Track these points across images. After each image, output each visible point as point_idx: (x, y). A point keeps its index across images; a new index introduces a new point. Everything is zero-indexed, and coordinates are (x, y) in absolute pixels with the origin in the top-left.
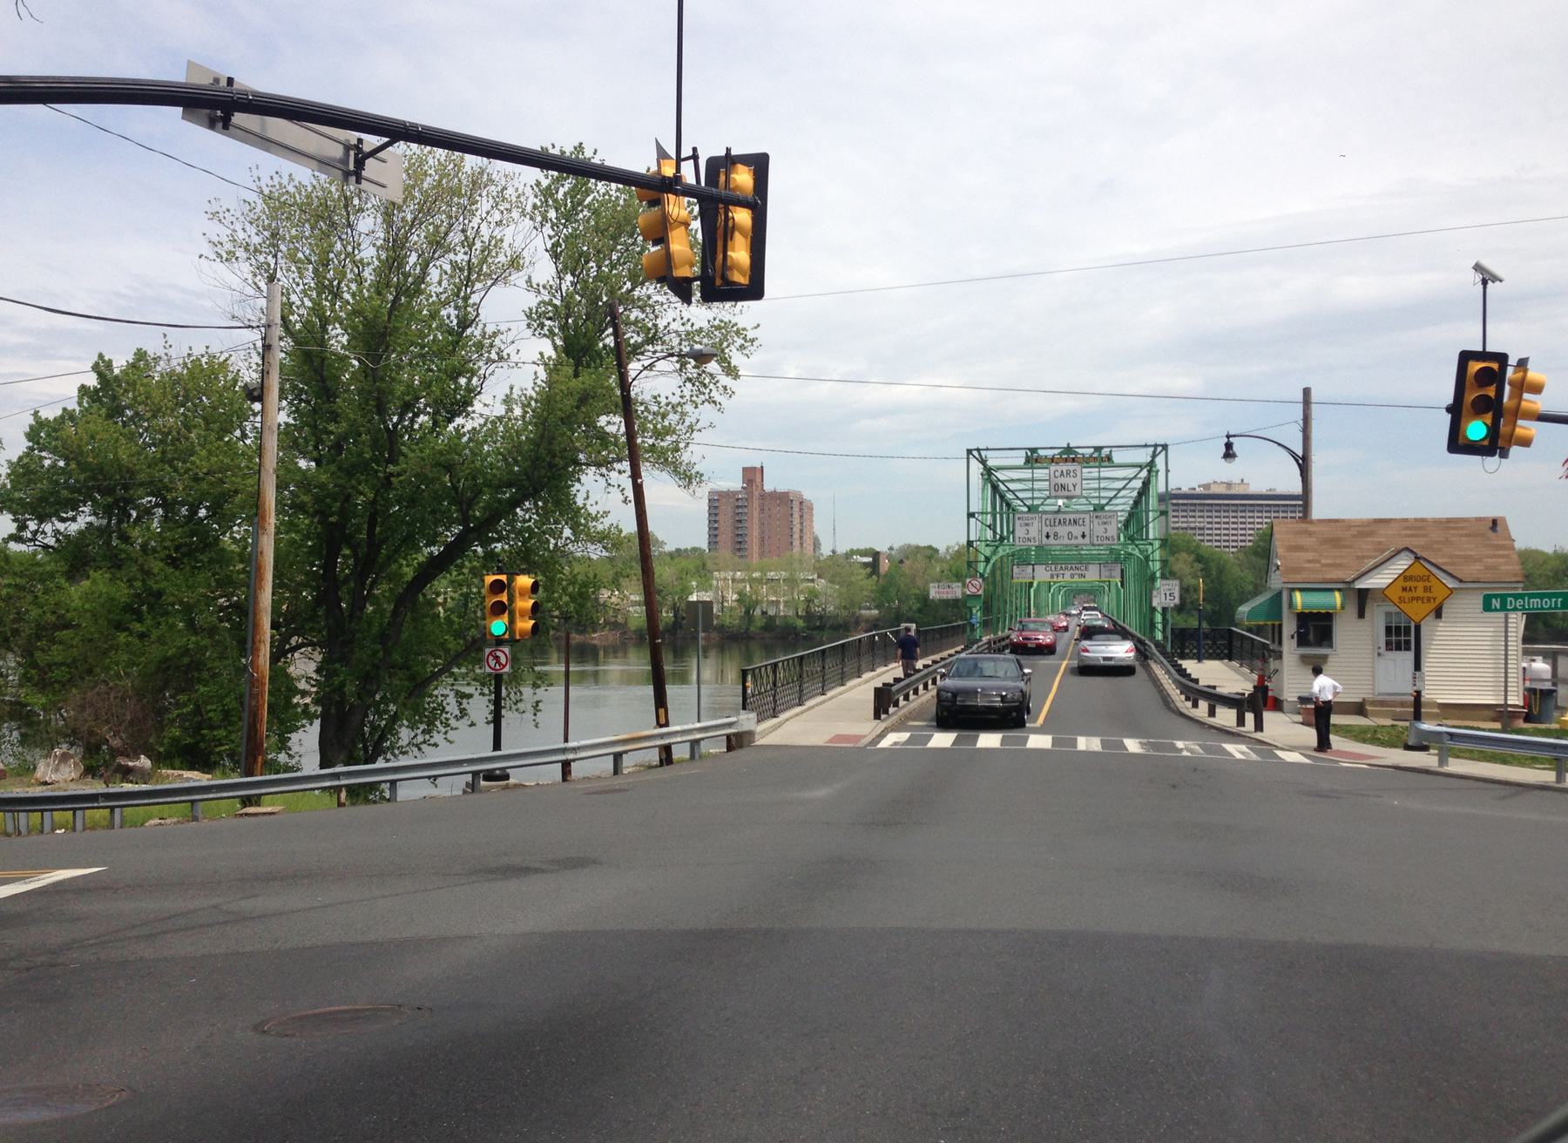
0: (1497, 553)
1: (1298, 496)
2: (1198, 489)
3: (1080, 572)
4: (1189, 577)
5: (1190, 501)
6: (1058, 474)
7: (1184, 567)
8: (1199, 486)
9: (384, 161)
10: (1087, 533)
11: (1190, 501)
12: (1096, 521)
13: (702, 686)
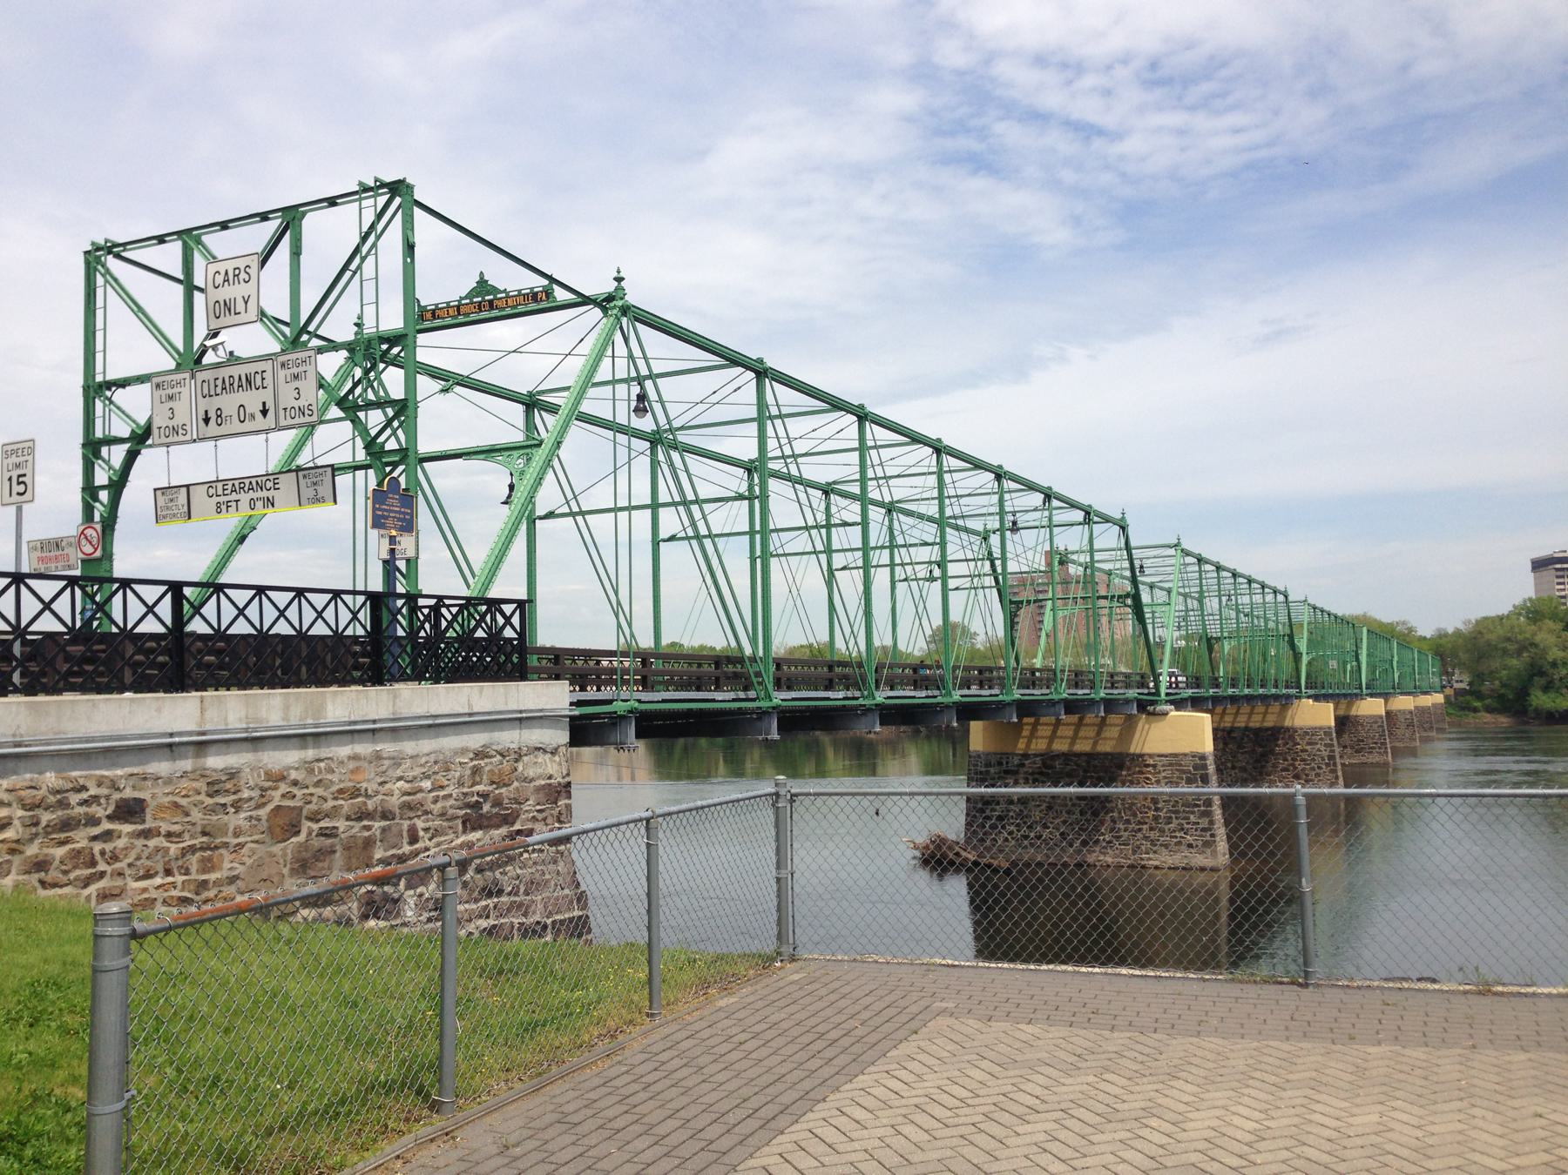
3: (265, 494)
6: (219, 279)
10: (269, 405)
12: (282, 373)
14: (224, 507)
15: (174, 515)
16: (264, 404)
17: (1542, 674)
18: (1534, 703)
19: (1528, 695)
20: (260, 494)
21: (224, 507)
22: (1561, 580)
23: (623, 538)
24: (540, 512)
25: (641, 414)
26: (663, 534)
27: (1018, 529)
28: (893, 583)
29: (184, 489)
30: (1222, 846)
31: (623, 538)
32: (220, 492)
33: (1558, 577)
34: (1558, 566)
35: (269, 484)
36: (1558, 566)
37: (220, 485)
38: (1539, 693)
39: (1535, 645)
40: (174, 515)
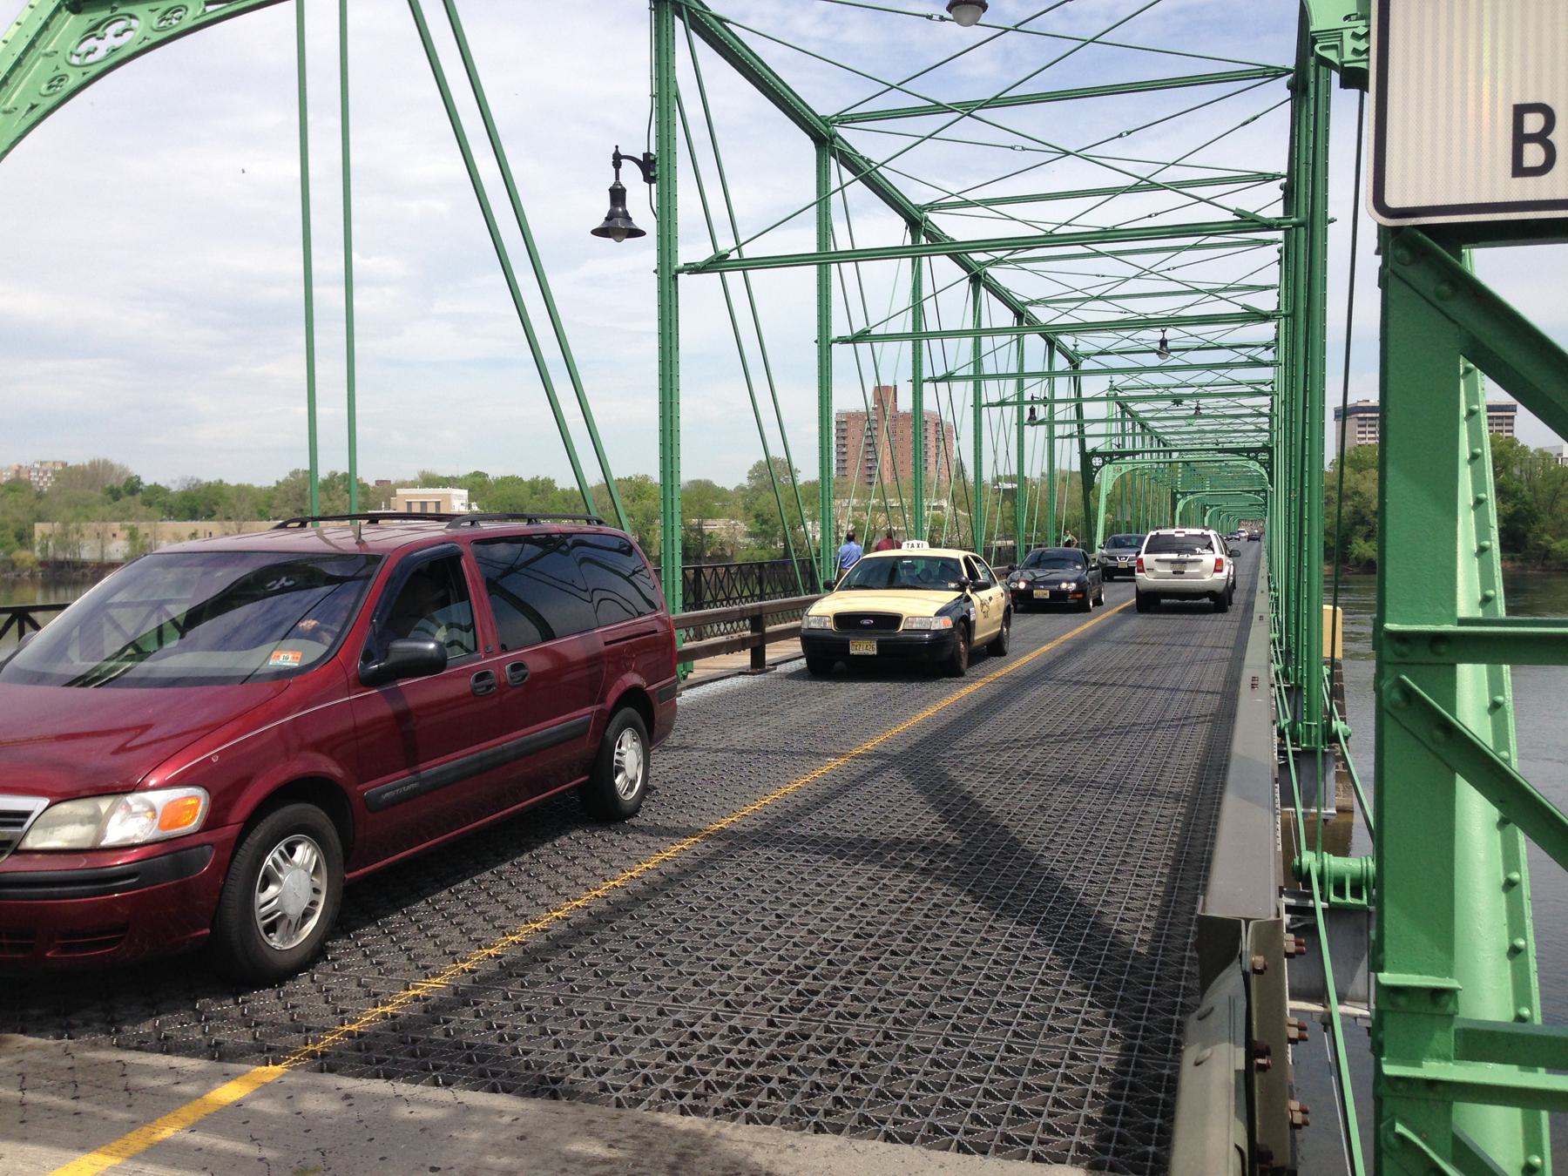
13: (1104, 403)
16: (617, 147)
17: (1363, 521)
18: (1356, 552)
19: (1350, 543)
22: (1363, 429)
23: (329, 297)
24: (680, 264)
26: (839, 328)
28: (978, 407)
30: (1365, 897)
31: (329, 297)
33: (1359, 426)
34: (1361, 415)
36: (1361, 415)
38: (1361, 542)
39: (1356, 493)
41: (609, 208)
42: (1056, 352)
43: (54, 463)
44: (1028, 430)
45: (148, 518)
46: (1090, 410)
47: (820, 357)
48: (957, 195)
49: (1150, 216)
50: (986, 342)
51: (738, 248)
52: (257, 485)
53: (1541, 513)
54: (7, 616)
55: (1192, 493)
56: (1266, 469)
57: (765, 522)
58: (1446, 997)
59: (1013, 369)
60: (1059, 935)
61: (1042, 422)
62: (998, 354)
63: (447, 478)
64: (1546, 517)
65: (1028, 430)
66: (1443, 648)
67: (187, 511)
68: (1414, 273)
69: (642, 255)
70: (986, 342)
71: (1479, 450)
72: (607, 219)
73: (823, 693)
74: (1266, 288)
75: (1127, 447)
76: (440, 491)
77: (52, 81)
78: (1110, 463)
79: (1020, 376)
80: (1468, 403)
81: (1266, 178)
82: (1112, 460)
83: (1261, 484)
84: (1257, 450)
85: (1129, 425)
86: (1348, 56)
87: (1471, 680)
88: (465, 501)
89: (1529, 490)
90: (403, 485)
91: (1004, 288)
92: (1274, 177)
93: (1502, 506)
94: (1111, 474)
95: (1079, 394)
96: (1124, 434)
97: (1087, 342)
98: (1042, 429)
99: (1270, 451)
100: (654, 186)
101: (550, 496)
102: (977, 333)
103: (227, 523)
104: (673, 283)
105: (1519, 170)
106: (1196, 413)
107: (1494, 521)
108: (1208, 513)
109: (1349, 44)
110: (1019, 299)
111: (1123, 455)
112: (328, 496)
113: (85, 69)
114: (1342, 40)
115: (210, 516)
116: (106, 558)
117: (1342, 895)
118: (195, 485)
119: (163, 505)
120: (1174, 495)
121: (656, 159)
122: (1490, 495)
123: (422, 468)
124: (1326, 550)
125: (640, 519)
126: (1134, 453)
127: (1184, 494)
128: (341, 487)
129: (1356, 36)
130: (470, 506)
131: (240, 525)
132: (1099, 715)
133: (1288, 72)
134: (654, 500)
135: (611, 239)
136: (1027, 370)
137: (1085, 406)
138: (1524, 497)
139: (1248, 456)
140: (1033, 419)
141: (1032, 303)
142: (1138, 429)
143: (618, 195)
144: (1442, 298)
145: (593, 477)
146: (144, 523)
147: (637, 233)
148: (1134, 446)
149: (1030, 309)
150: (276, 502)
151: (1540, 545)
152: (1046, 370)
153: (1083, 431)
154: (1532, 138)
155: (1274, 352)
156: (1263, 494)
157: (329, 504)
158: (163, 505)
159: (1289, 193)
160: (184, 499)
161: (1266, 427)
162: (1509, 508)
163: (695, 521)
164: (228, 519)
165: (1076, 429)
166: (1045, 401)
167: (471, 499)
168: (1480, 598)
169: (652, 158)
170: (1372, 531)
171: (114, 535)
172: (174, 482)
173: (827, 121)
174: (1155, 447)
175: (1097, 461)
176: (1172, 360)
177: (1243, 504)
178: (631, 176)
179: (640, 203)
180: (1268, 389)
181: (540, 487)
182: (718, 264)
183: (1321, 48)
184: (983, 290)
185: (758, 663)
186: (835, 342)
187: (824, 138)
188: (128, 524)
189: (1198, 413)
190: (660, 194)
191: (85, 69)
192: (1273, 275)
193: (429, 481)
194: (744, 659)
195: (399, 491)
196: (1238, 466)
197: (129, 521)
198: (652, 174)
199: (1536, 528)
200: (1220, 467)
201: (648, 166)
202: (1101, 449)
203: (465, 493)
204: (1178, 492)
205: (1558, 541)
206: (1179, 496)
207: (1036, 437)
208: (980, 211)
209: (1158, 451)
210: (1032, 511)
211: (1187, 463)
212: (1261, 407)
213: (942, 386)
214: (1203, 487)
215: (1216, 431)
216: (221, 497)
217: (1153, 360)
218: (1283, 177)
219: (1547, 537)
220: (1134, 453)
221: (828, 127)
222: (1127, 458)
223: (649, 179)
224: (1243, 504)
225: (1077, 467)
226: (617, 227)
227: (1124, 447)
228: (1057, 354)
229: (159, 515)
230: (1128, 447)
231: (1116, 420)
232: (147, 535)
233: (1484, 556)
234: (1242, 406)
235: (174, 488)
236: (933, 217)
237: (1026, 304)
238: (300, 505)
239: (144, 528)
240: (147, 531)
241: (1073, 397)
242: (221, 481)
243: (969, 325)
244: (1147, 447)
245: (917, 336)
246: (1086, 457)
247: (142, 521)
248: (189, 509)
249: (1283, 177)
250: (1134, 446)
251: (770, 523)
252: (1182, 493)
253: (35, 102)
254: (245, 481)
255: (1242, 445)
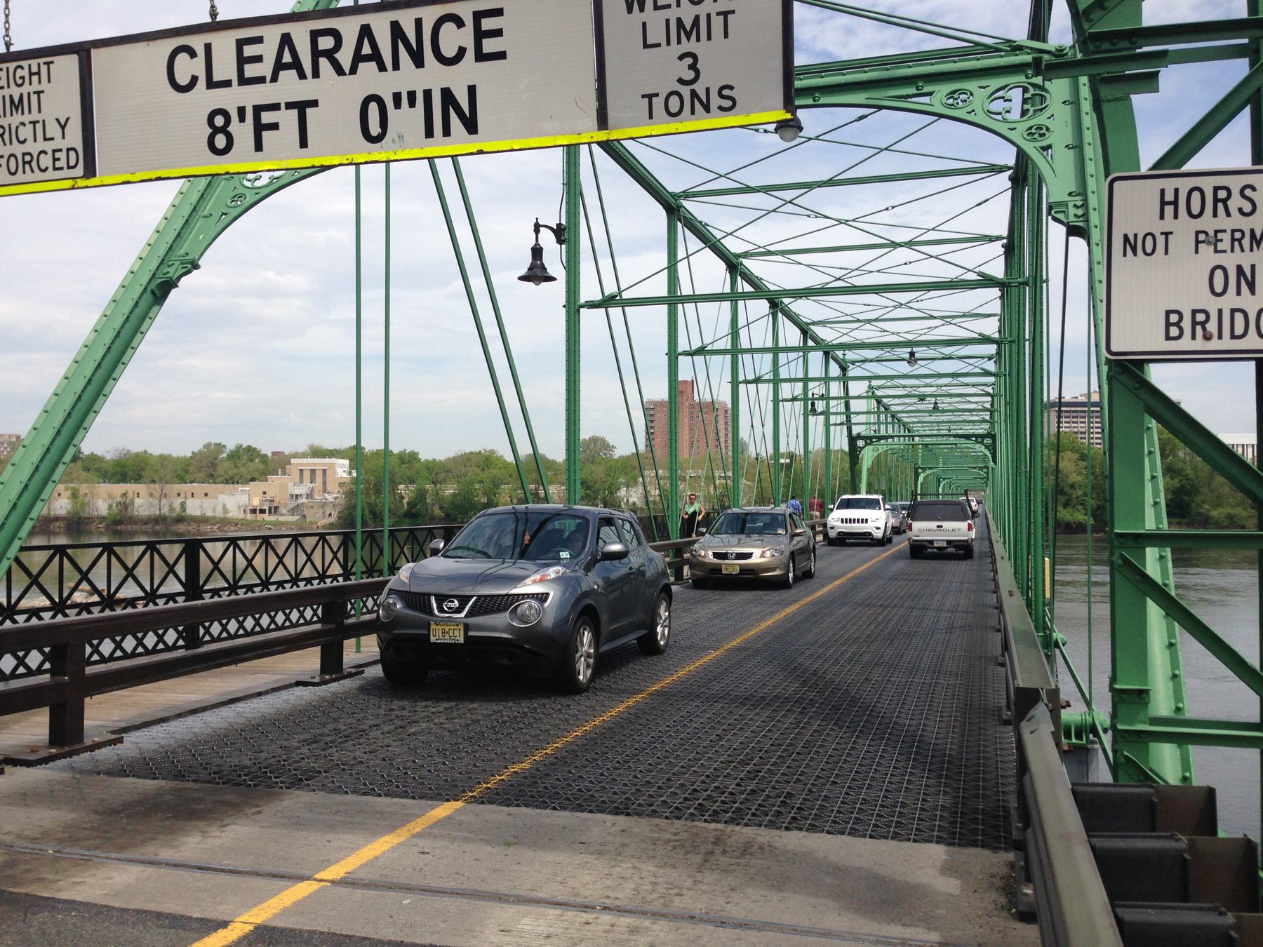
0: (614, 588)
1: (675, 292)
2: (1080, 398)
3: (433, 76)
4: (1074, 474)
5: (1073, 409)
7: (1068, 464)
8: (1081, 396)
9: (68, 119)
11: (1073, 409)
13: (865, 400)
14: (243, 132)
15: (28, 161)
20: (409, 78)
21: (243, 132)
24: (582, 301)
25: (789, 133)
26: (682, 345)
27: (916, 360)
28: (776, 401)
29: (70, 63)
30: (1084, 739)
32: (225, 67)
35: (452, 39)
37: (224, 45)
40: (28, 161)
41: (531, 262)
42: (831, 361)
43: (10, 436)
44: (812, 419)
45: (86, 481)
46: (855, 405)
47: (670, 365)
48: (763, 247)
49: (906, 264)
50: (782, 357)
51: (620, 293)
52: (174, 455)
53: (1202, 487)
54: (100, 549)
55: (930, 468)
56: (989, 450)
57: (589, 488)
58: (1144, 695)
59: (800, 375)
60: (841, 799)
61: (821, 413)
62: (791, 366)
63: (331, 451)
64: (1205, 490)
65: (812, 419)
66: (1140, 540)
67: (119, 476)
68: (1123, 378)
69: (555, 292)
70: (782, 357)
71: (1188, 775)
72: (529, 269)
73: (865, 550)
74: (989, 316)
75: (882, 432)
76: (327, 460)
77: (234, 197)
78: (869, 444)
79: (806, 380)
80: (1149, 447)
81: (991, 239)
82: (872, 442)
83: (984, 461)
84: (983, 436)
85: (882, 417)
86: (1072, 218)
87: (1151, 553)
88: (347, 469)
89: (1192, 469)
90: (296, 455)
91: (795, 313)
92: (998, 238)
93: (1170, 482)
94: (870, 453)
95: (847, 393)
96: (879, 423)
97: (851, 355)
98: (822, 418)
99: (993, 437)
100: (564, 246)
101: (416, 465)
102: (776, 350)
103: (152, 486)
104: (577, 314)
105: (1168, 338)
106: (934, 408)
107: (1161, 488)
108: (942, 485)
109: (1072, 211)
110: (805, 320)
111: (880, 438)
112: (235, 463)
113: (257, 191)
114: (1067, 208)
115: (138, 478)
116: (52, 513)
117: (1070, 738)
118: (125, 455)
119: (98, 470)
120: (916, 470)
121: (565, 228)
122: (1159, 474)
123: (310, 442)
124: (372, 861)
125: (488, 484)
126: (886, 438)
127: (924, 469)
128: (245, 458)
129: (1075, 206)
130: (350, 473)
131: (163, 487)
132: (890, 626)
133: (1009, 168)
134: (500, 469)
135: (532, 283)
136: (810, 376)
137: (852, 402)
138: (1187, 474)
139: (976, 441)
140: (814, 411)
141: (814, 323)
142: (890, 420)
143: (537, 252)
144: (1137, 389)
145: (525, 449)
146: (84, 485)
147: (552, 279)
148: (887, 432)
149: (812, 327)
150: (191, 468)
151: (1201, 513)
152: (823, 376)
153: (850, 421)
154: (1173, 324)
155: (995, 362)
156: (985, 470)
157: (235, 471)
158: (98, 470)
159: (1011, 250)
160: (117, 465)
161: (988, 418)
162: (1176, 483)
163: (533, 486)
164: (153, 482)
165: (845, 419)
166: (822, 397)
167: (351, 467)
168: (1158, 557)
169: (563, 227)
170: (1069, 500)
171: (59, 495)
172: (109, 452)
173: (676, 196)
174: (902, 433)
175: (860, 443)
176: (919, 369)
177: (969, 477)
178: (547, 239)
179: (554, 261)
180: (990, 390)
181: (407, 458)
182: (607, 302)
183: (1055, 212)
184: (780, 315)
185: (332, 665)
186: (681, 354)
187: (673, 207)
188: (70, 485)
189: (936, 409)
190: (568, 252)
191: (257, 191)
192: (996, 307)
193: (317, 453)
194: (309, 661)
195: (293, 461)
196: (966, 448)
197: (71, 483)
198: (563, 238)
199: (1198, 499)
200: (952, 448)
201: (559, 232)
202: (863, 434)
203: (346, 462)
204: (919, 467)
205: (1216, 510)
206: (920, 471)
207: (816, 423)
208: (779, 258)
209: (904, 436)
210: (815, 478)
211: (926, 445)
212: (985, 402)
213: (752, 387)
214: (938, 464)
215: (949, 422)
216: (147, 464)
217: (904, 368)
218: (1004, 238)
219: (1207, 507)
220: (886, 438)
221: (676, 200)
222: (889, 440)
223: (560, 241)
224: (969, 477)
225: (846, 448)
226: (537, 274)
227: (879, 432)
228: (832, 362)
229: (96, 478)
230: (882, 432)
231: (874, 413)
232: (86, 494)
233: (1157, 506)
234: (969, 402)
235: (108, 457)
236: (746, 262)
237: (810, 324)
238: (211, 471)
239: (84, 489)
240: (87, 491)
241: (842, 395)
242: (146, 452)
243: (769, 344)
244: (896, 433)
245: (735, 351)
246: (852, 440)
247: (82, 483)
248: (121, 474)
249: (1004, 238)
250: (887, 432)
251: (593, 489)
252: (922, 468)
253: (225, 212)
254: (166, 452)
255: (971, 432)
